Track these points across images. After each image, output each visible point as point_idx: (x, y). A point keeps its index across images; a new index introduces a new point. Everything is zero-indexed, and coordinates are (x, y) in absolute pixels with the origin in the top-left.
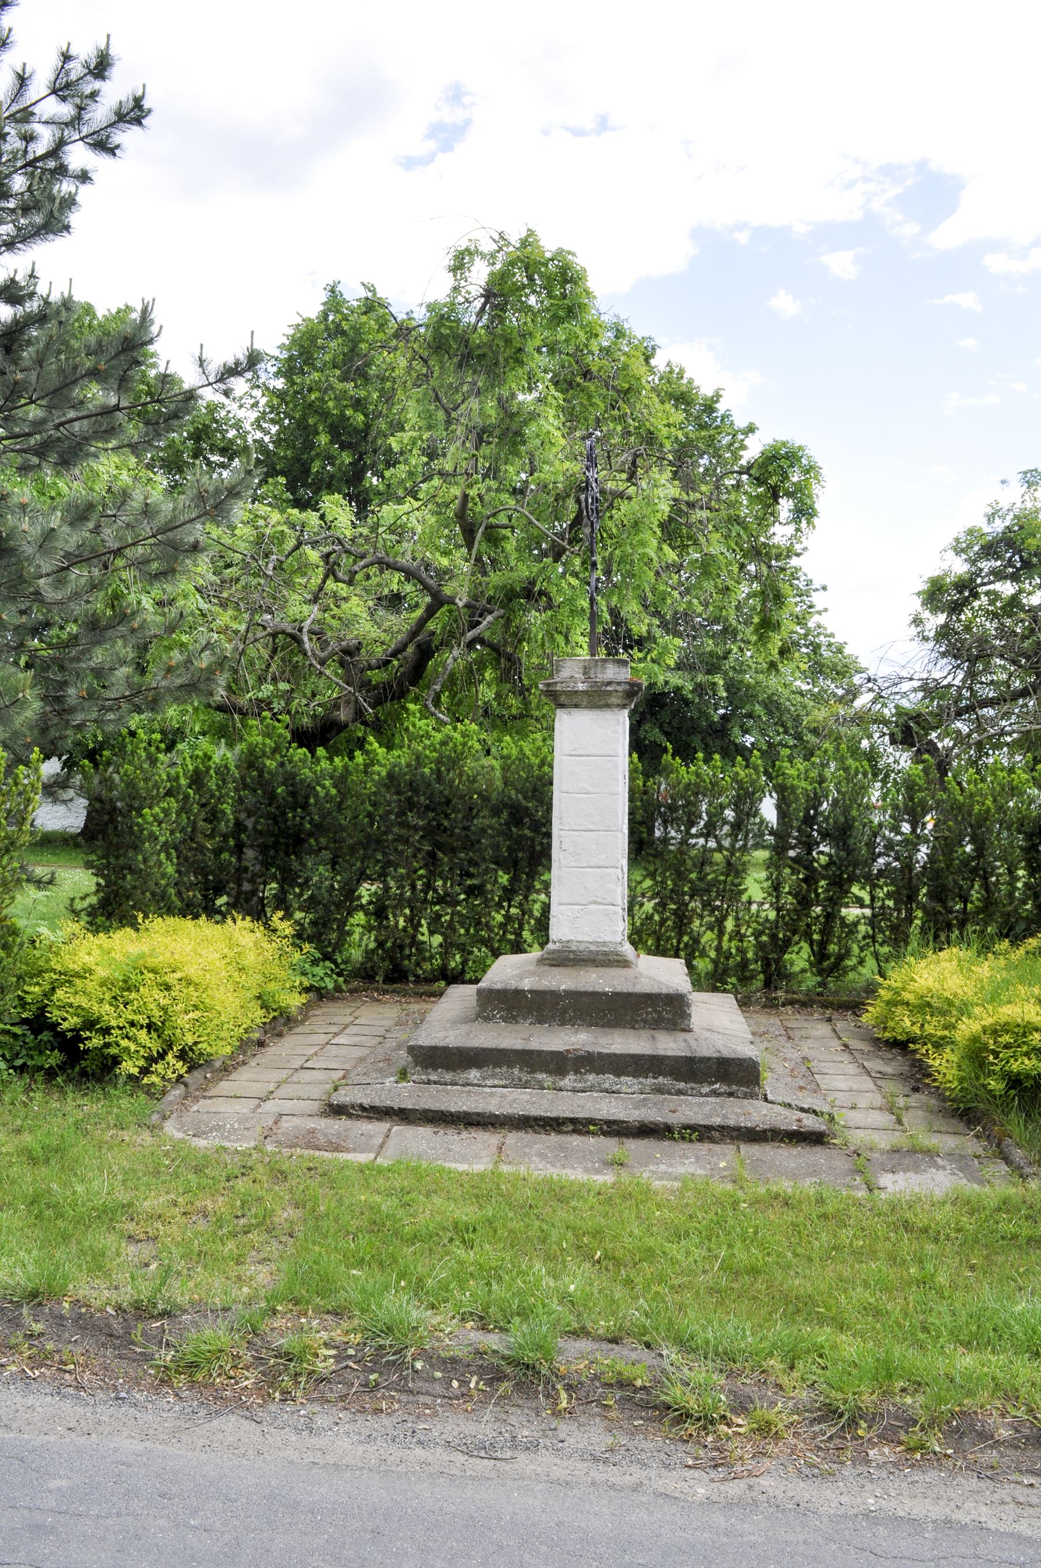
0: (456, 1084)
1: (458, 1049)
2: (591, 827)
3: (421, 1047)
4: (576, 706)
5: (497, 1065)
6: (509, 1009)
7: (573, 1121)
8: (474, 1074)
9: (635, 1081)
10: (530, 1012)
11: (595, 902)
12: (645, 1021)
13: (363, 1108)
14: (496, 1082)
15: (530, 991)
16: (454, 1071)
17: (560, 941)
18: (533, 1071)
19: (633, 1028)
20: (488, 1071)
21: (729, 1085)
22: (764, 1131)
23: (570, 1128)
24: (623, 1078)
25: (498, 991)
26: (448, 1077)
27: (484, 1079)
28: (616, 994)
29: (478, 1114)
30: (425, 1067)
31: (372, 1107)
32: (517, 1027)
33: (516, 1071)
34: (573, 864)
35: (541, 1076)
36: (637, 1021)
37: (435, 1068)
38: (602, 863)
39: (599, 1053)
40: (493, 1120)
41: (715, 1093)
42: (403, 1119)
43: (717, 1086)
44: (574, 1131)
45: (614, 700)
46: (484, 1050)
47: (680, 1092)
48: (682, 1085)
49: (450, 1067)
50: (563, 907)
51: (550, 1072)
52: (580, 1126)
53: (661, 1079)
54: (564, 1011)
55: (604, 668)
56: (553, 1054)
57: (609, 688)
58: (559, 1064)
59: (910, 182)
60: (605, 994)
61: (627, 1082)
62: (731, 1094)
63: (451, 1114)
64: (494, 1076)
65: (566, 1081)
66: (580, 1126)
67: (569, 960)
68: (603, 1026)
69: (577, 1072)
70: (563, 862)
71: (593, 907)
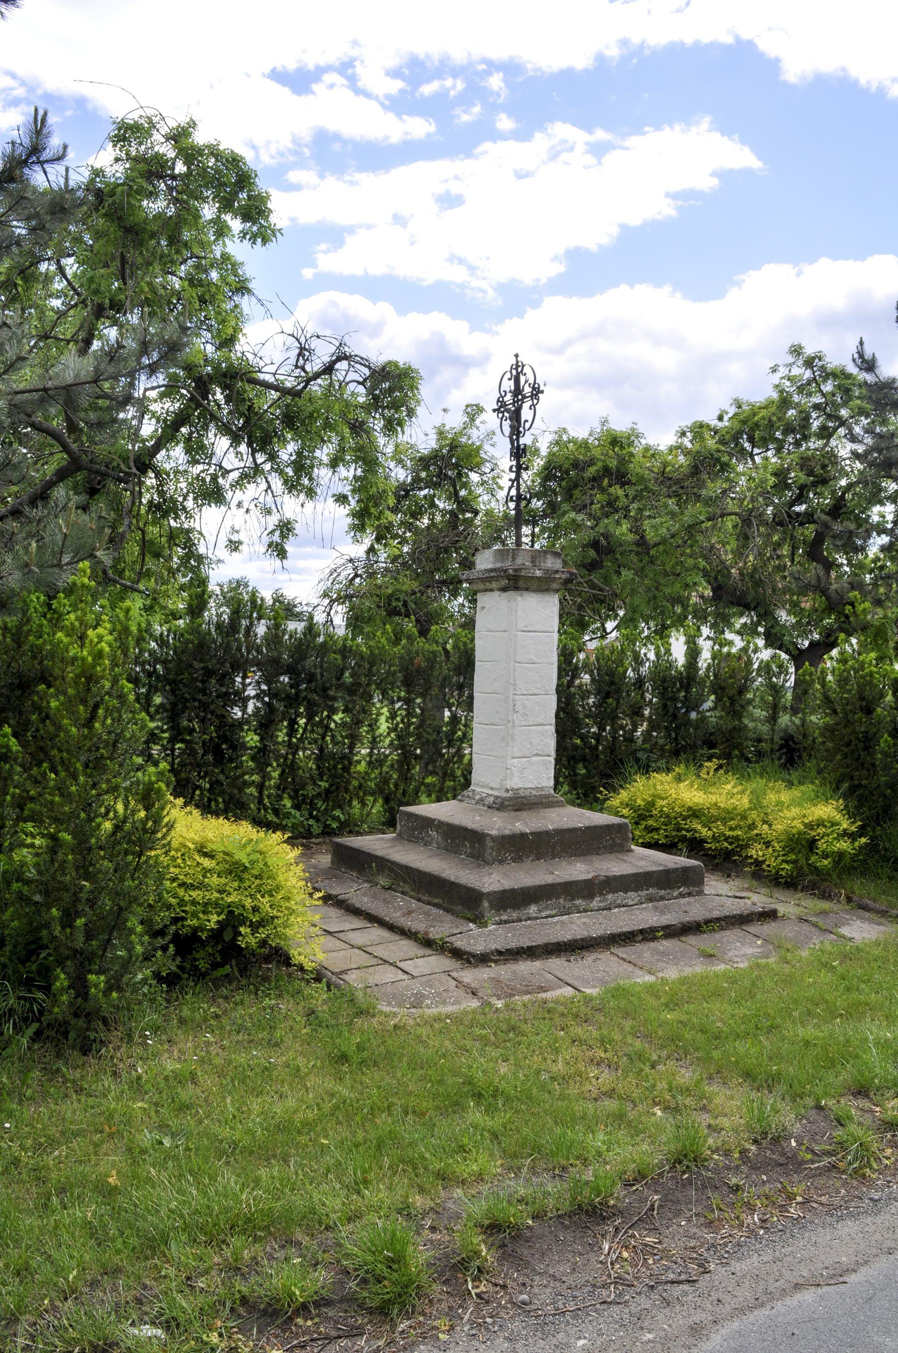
0: (520, 920)
1: (522, 889)
2: (536, 692)
4: (527, 589)
5: (549, 898)
7: (641, 931)
8: (533, 909)
11: (537, 755)
12: (604, 847)
13: (500, 953)
15: (531, 834)
17: (512, 789)
20: (543, 904)
22: (748, 915)
23: (641, 937)
25: (509, 836)
26: (515, 915)
27: (540, 911)
28: (588, 828)
29: (582, 940)
30: (498, 910)
31: (507, 950)
32: (524, 865)
35: (578, 902)
38: (543, 722)
40: (592, 942)
41: (681, 895)
42: (529, 956)
44: (643, 940)
45: (555, 586)
46: (540, 887)
47: (662, 898)
48: (662, 892)
51: (584, 898)
52: (648, 935)
56: (585, 881)
57: (557, 576)
58: (586, 890)
59: (69, 113)
60: (580, 829)
61: (632, 897)
63: (565, 944)
64: (546, 908)
66: (648, 935)
67: (525, 805)
69: (601, 894)
71: (535, 759)
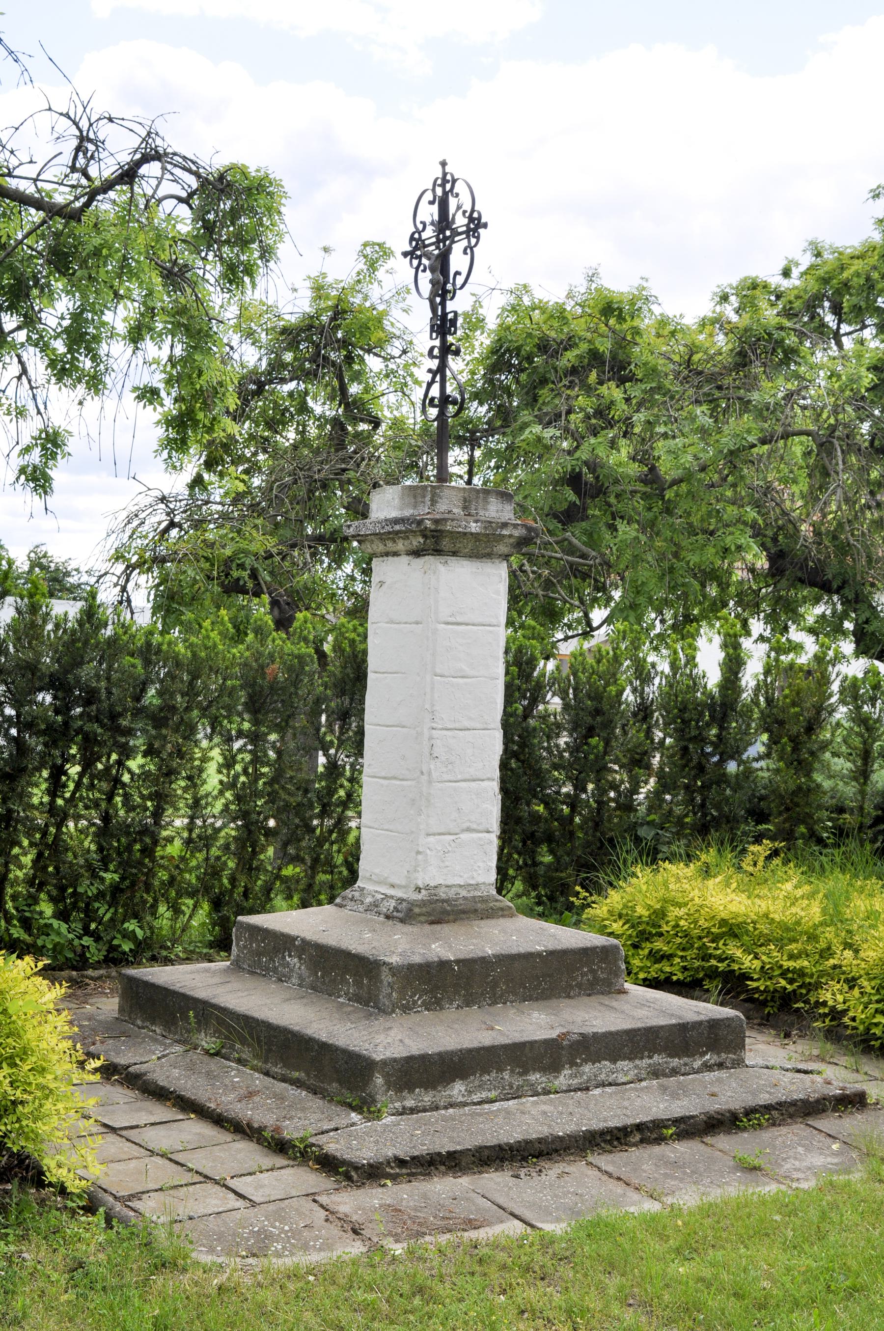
0: (437, 1108)
1: (440, 1054)
2: (467, 724)
3: (395, 1060)
4: (454, 554)
5: (486, 1071)
6: (432, 991)
8: (458, 1089)
9: (631, 1065)
10: (456, 992)
11: (469, 830)
12: (580, 986)
13: (401, 1162)
14: (484, 1095)
15: (458, 962)
16: (434, 1088)
17: (427, 888)
18: (526, 1072)
19: (569, 997)
21: (718, 1054)
23: (638, 1137)
24: (621, 1064)
25: (420, 966)
26: (427, 1098)
27: (470, 1092)
28: (551, 953)
29: (540, 1141)
30: (399, 1090)
31: (413, 1158)
33: (506, 1075)
34: (446, 777)
35: (534, 1077)
36: (571, 987)
37: (411, 1090)
39: (595, 1034)
40: (557, 1145)
41: (707, 1067)
42: (450, 1168)
43: (708, 1057)
44: (642, 1141)
45: (502, 549)
46: (470, 1051)
47: (674, 1072)
48: (675, 1062)
49: (430, 1084)
50: (431, 839)
51: (544, 1070)
52: (649, 1133)
53: (656, 1058)
54: (495, 985)
55: (486, 502)
57: (505, 532)
60: (539, 954)
61: (625, 1069)
62: (721, 1066)
63: (511, 1147)
64: (480, 1087)
65: (562, 1078)
66: (649, 1133)
67: (448, 913)
68: (537, 999)
69: (573, 1064)
70: (435, 775)
71: (465, 836)
